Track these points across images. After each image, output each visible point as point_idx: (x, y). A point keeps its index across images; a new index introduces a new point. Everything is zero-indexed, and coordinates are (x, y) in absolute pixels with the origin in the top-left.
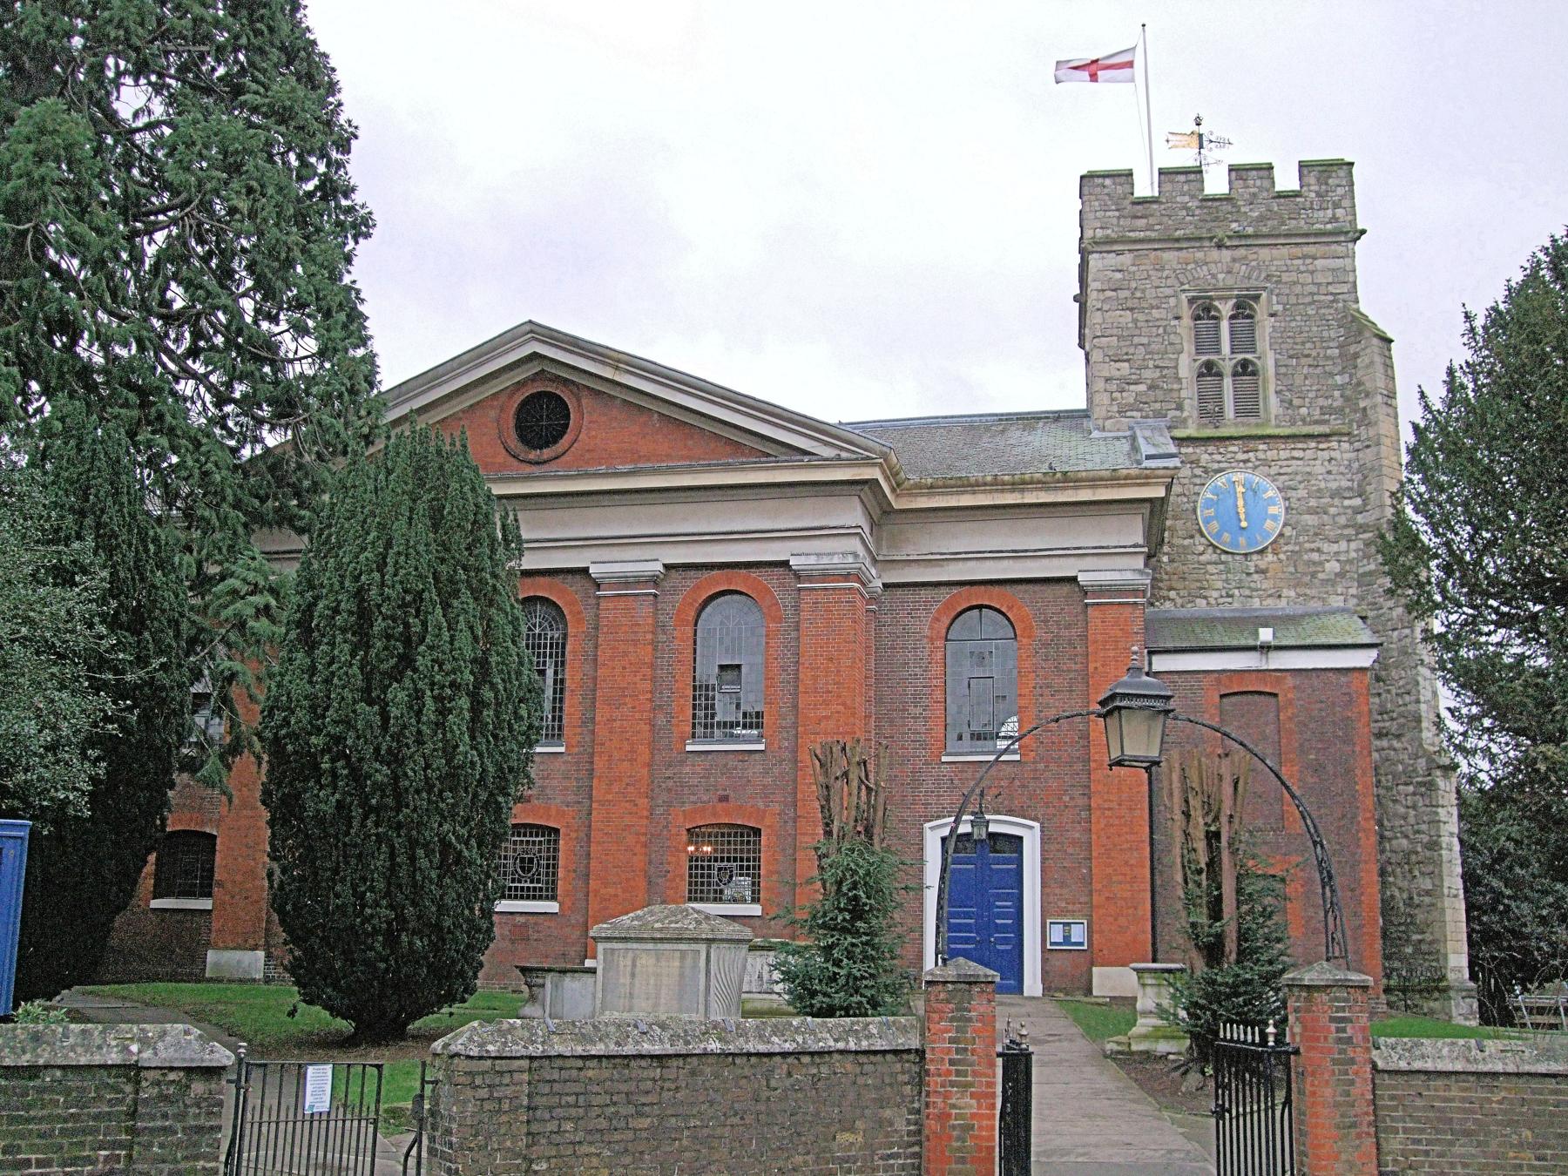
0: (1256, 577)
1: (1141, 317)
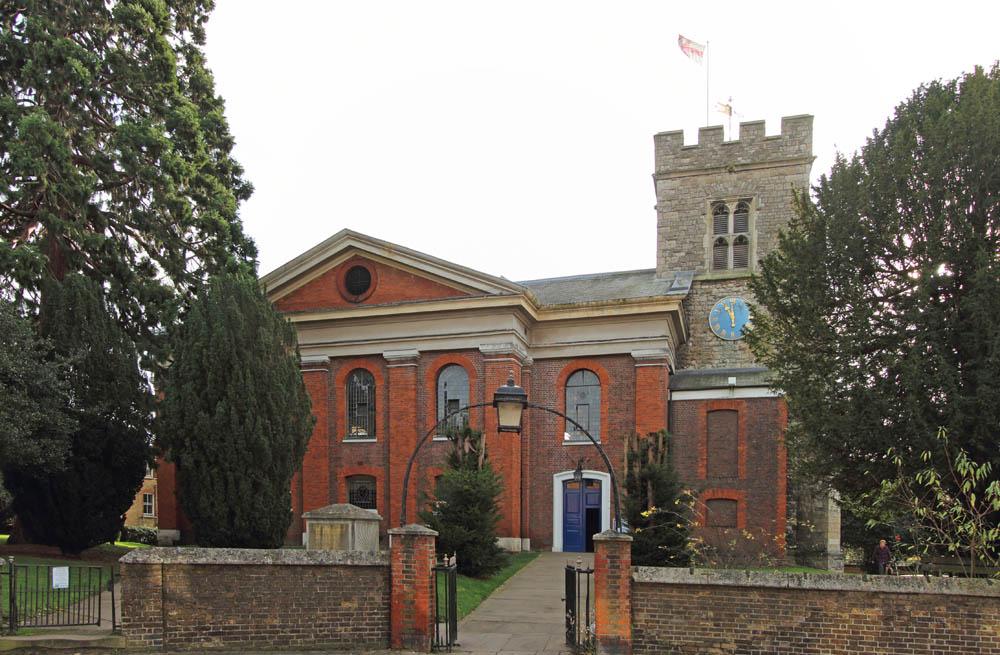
0: (739, 352)
1: (684, 215)
